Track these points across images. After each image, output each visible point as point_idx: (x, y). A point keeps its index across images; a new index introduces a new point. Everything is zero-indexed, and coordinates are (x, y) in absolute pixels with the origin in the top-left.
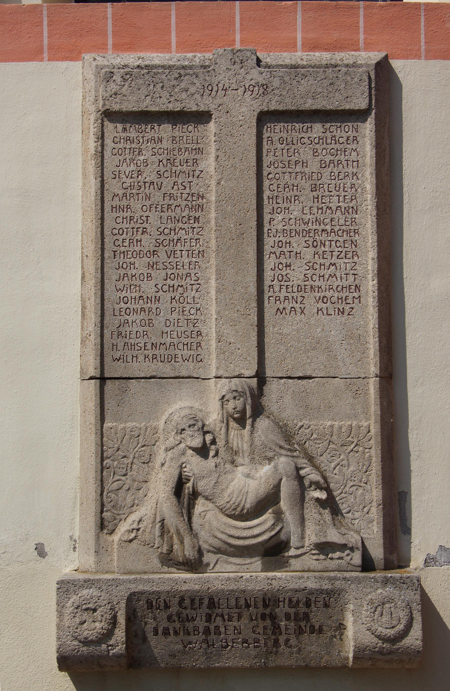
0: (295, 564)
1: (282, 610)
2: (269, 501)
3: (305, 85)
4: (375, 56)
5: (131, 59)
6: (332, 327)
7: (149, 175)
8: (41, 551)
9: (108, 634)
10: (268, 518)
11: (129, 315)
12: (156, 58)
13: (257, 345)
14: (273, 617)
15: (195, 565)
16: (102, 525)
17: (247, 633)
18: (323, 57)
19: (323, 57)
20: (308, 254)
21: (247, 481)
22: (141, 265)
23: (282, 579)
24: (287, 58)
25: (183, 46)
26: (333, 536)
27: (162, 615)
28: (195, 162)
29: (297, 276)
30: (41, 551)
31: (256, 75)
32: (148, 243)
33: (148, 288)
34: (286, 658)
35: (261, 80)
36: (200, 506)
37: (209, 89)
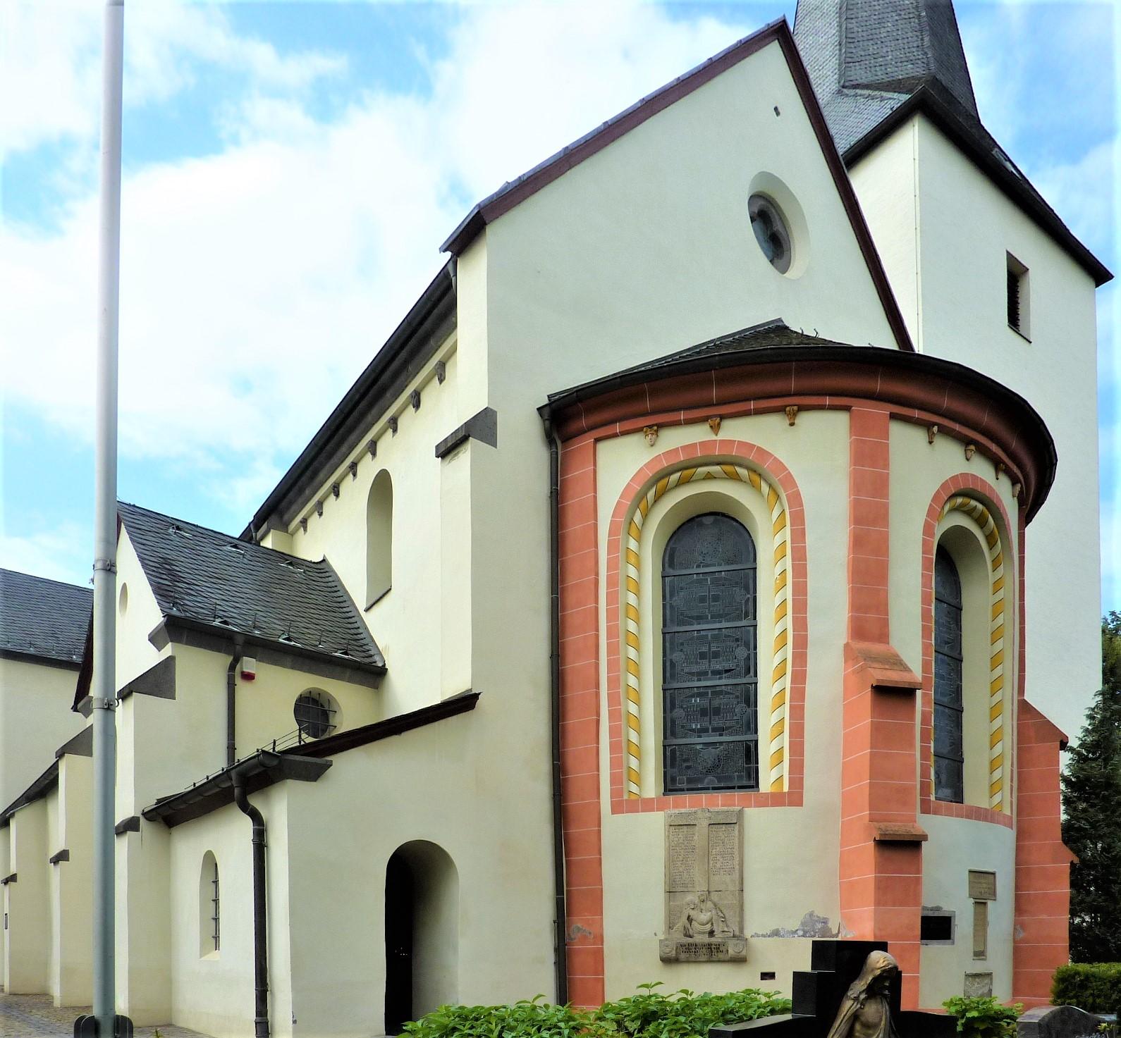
0: (716, 936)
1: (713, 947)
2: (711, 921)
3: (720, 817)
4: (739, 808)
5: (677, 811)
6: (728, 878)
7: (681, 841)
8: (655, 934)
9: (671, 951)
10: (709, 925)
11: (1016, 440)
12: (683, 810)
13: (509, 181)
14: (711, 949)
15: (691, 937)
16: (670, 928)
17: (705, 952)
18: (725, 808)
19: (725, 808)
20: (721, 860)
21: (704, 917)
22: (679, 863)
23: (713, 940)
24: (716, 809)
25: (690, 807)
26: (726, 929)
27: (684, 948)
28: (693, 837)
29: (718, 866)
30: (655, 934)
31: (708, 815)
32: (681, 858)
33: (681, 869)
34: (714, 958)
35: (709, 816)
36: (693, 922)
37: (695, 819)
